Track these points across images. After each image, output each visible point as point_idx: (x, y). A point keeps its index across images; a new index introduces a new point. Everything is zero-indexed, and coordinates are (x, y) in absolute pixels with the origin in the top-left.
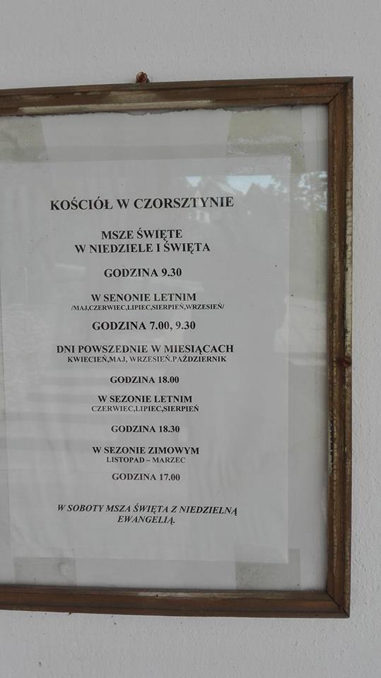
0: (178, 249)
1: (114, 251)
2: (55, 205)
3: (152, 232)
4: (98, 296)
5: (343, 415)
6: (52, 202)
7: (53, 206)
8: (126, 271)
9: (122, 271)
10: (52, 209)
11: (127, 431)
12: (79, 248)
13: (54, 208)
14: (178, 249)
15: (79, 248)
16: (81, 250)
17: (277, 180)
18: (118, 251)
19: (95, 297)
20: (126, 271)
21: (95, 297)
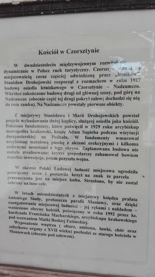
0: (8, 94)
1: (28, 83)
2: (41, 52)
3: (8, 93)
4: (18, 167)
5: (114, 9)
6: (39, 51)
7: (40, 53)
8: (27, 82)
9: (53, 53)
10: (39, 54)
11: (53, 201)
12: (16, 192)
13: (40, 54)
14: (8, 94)
15: (16, 192)
16: (16, 66)
17: (143, 65)
18: (74, 51)
19: (15, 65)
20: (27, 82)
21: (15, 65)
